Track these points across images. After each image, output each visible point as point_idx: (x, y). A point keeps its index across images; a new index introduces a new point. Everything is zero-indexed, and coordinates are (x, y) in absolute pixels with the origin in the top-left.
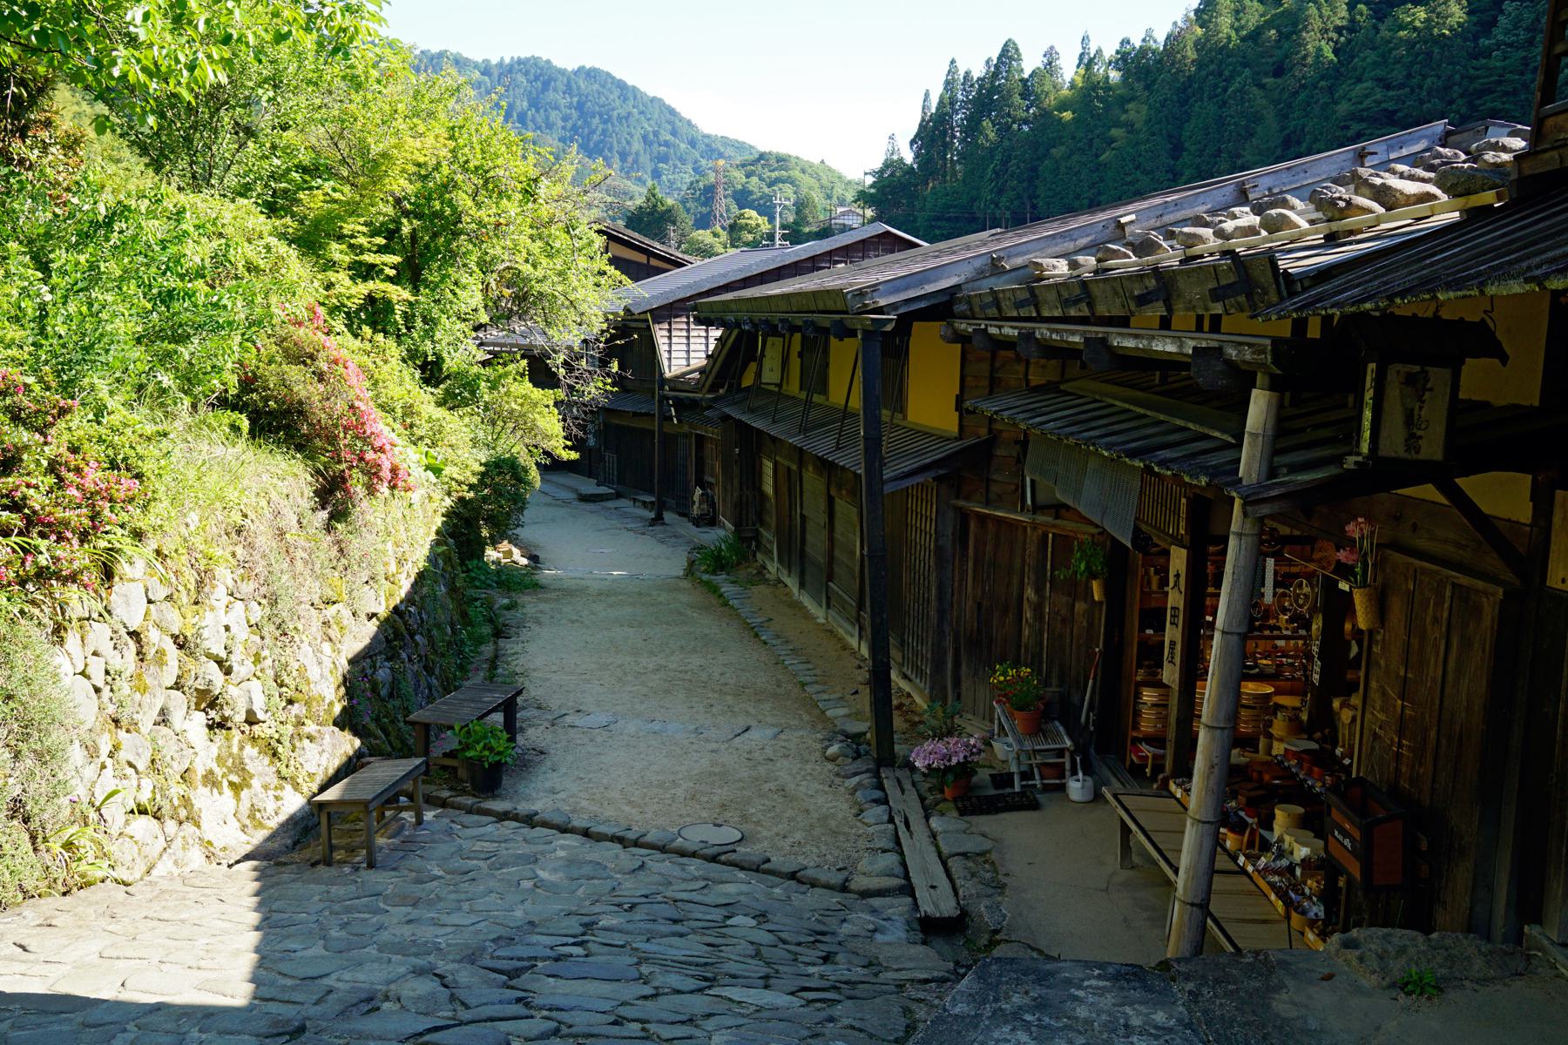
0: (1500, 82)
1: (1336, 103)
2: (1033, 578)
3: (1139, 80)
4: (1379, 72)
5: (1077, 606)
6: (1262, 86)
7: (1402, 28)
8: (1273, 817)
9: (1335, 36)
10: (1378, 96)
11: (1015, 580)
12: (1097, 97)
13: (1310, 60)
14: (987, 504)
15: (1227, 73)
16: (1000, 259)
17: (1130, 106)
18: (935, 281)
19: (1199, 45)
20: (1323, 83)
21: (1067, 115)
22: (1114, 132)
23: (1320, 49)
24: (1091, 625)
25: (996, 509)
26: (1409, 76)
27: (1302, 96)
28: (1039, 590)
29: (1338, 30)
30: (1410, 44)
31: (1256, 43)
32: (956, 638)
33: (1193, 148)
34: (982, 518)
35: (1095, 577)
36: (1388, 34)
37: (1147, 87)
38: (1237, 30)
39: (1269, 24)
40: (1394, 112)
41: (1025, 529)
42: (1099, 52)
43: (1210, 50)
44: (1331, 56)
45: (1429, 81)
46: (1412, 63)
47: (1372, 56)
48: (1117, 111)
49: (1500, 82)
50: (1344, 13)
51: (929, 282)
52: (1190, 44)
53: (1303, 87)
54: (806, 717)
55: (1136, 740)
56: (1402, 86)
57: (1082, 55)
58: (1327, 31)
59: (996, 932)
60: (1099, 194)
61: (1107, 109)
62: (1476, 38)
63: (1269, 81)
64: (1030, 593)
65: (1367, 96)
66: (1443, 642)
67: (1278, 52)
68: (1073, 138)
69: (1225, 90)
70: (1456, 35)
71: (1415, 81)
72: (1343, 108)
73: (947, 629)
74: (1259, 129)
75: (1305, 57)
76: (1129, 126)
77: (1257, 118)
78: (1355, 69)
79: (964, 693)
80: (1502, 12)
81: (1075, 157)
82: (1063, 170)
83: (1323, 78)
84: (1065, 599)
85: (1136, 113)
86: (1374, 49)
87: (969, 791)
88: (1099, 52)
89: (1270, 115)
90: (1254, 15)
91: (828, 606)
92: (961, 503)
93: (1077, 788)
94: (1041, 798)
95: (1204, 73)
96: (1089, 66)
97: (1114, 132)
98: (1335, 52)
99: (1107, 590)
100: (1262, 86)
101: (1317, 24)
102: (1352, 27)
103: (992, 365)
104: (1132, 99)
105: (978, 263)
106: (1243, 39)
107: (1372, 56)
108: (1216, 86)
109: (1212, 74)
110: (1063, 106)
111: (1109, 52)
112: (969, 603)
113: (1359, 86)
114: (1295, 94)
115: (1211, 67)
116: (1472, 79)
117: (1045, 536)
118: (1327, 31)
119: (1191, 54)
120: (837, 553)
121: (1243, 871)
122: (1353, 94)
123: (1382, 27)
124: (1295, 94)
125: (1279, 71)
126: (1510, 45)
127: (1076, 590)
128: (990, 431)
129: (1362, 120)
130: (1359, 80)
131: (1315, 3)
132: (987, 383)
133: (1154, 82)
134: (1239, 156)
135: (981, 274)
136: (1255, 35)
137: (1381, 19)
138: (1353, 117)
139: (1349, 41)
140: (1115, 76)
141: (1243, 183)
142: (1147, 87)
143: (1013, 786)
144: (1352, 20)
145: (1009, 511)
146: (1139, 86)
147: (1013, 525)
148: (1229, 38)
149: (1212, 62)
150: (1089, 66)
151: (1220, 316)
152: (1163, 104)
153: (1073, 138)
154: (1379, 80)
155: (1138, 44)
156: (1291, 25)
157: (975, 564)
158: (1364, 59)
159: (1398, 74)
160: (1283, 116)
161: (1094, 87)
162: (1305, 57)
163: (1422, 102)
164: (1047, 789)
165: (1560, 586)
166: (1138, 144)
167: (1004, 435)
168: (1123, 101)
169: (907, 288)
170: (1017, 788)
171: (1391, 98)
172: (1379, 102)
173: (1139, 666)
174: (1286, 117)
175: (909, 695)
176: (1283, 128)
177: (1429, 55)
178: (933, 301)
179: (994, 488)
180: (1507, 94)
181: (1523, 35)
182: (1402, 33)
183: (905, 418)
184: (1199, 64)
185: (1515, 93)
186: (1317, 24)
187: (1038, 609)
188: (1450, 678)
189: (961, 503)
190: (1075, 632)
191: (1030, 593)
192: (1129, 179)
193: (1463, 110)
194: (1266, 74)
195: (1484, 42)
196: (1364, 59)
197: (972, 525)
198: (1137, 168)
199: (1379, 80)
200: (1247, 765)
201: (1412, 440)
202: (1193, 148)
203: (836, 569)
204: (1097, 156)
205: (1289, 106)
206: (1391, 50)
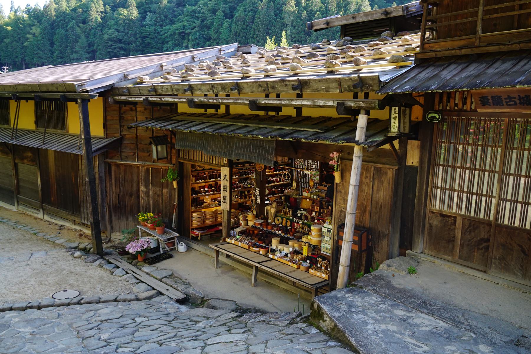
0: (149, 35)
1: (103, 35)
2: (144, 184)
3: (35, 19)
4: (115, 27)
5: (164, 191)
6: (79, 27)
7: (120, 14)
8: (271, 241)
9: (101, 14)
10: (116, 34)
11: (135, 185)
12: (20, 23)
13: (93, 20)
14: (122, 160)
15: (67, 21)
16: (128, 75)
17: (33, 28)
18: (106, 81)
19: (56, 10)
20: (99, 28)
21: (9, 28)
22: (28, 36)
23: (96, 17)
24: (170, 196)
25: (126, 161)
26: (124, 29)
27: (93, 31)
28: (146, 186)
29: (101, 12)
30: (124, 20)
31: (75, 12)
32: (109, 208)
33: (58, 44)
34: (118, 165)
35: (174, 180)
36: (117, 16)
37: (38, 22)
38: (68, 7)
39: (79, 7)
40: (121, 40)
41: (138, 167)
42: (19, 7)
43: (60, 12)
44: (100, 20)
45: (130, 32)
46: (125, 26)
47: (113, 22)
48: (28, 29)
49: (149, 35)
50: (103, 7)
51: (104, 82)
52: (53, 9)
53: (92, 28)
54: (49, 246)
55: (193, 229)
56: (123, 32)
57: (11, 8)
58: (98, 12)
59: (203, 297)
60: (25, 56)
61: (25, 27)
62: (141, 21)
63: (81, 25)
64: (143, 188)
65: (113, 34)
66: (371, 183)
67: (83, 16)
68: (13, 36)
69: (67, 26)
70: (136, 19)
71: (126, 31)
72: (106, 37)
73: (105, 205)
74: (80, 40)
75: (92, 19)
76: (34, 34)
77: (78, 37)
78: (108, 25)
79: (114, 226)
80: (147, 15)
81: (14, 43)
82: (9, 47)
83: (98, 26)
84: (158, 189)
85: (36, 30)
86: (113, 20)
87: (153, 256)
88: (19, 7)
89: (83, 36)
90: (74, 4)
91: (18, 204)
92: (109, 160)
93: (182, 248)
94: (171, 253)
95: (59, 20)
96: (15, 12)
97: (28, 36)
98: (101, 19)
99: (178, 184)
100: (79, 27)
101: (95, 9)
102: (105, 12)
103: (120, 112)
104: (34, 25)
105: (120, 76)
106: (71, 10)
107: (113, 22)
108: (63, 25)
109: (61, 20)
110: (7, 24)
111: (23, 7)
112: (114, 195)
113: (110, 30)
114: (90, 30)
115: (62, 18)
116: (142, 33)
117: (148, 170)
118: (98, 12)
119: (54, 13)
120: (21, 184)
121: (272, 259)
122: (109, 33)
123: (115, 13)
124: (90, 30)
125: (84, 22)
126: (151, 25)
127: (168, 185)
128: (121, 135)
129: (112, 41)
130: (110, 29)
131: (93, 2)
132: (118, 118)
133: (41, 20)
134: (74, 48)
135: (121, 80)
136: (74, 10)
137: (114, 11)
138: (110, 40)
139: (105, 16)
140: (26, 16)
141: (193, 56)
142: (38, 22)
143: (160, 251)
144: (105, 10)
145: (132, 162)
146: (36, 21)
147: (131, 166)
148: (66, 9)
149: (61, 16)
150: (15, 12)
151: (368, 93)
152: (46, 28)
153: (13, 36)
154: (116, 29)
155: (33, 7)
156: (86, 9)
157: (115, 181)
158: (111, 22)
159: (121, 28)
160: (87, 37)
161: (19, 20)
162: (92, 19)
163: (129, 38)
164: (171, 250)
165: (411, 164)
166: (37, 41)
167: (127, 136)
168: (30, 26)
169: (97, 84)
170: (162, 252)
171: (120, 35)
172: (117, 36)
173: (192, 206)
174: (88, 37)
175: (81, 231)
176: (87, 41)
177: (129, 24)
178: (106, 89)
179: (123, 154)
180: (151, 38)
181: (154, 23)
182: (121, 16)
183: (68, 132)
184: (57, 17)
185: (153, 38)
186: (95, 9)
187: (147, 193)
188: (375, 192)
189: (109, 160)
190: (164, 199)
191: (143, 188)
192: (36, 52)
193: (141, 41)
194: (80, 23)
195: (144, 23)
196: (111, 22)
197: (113, 168)
198: (39, 49)
199: (116, 29)
200: (246, 229)
201: (405, 130)
202: (58, 44)
203: (21, 190)
204: (22, 44)
205: (89, 34)
206: (118, 21)
